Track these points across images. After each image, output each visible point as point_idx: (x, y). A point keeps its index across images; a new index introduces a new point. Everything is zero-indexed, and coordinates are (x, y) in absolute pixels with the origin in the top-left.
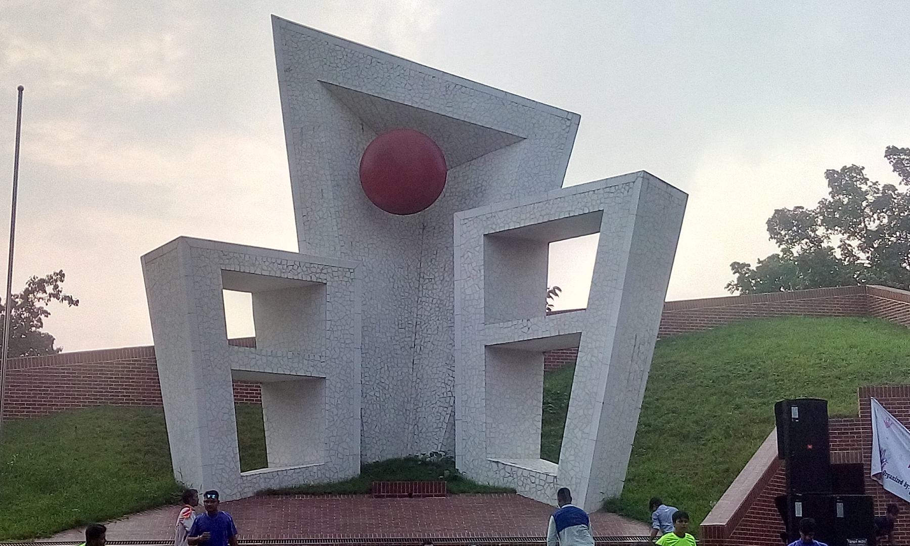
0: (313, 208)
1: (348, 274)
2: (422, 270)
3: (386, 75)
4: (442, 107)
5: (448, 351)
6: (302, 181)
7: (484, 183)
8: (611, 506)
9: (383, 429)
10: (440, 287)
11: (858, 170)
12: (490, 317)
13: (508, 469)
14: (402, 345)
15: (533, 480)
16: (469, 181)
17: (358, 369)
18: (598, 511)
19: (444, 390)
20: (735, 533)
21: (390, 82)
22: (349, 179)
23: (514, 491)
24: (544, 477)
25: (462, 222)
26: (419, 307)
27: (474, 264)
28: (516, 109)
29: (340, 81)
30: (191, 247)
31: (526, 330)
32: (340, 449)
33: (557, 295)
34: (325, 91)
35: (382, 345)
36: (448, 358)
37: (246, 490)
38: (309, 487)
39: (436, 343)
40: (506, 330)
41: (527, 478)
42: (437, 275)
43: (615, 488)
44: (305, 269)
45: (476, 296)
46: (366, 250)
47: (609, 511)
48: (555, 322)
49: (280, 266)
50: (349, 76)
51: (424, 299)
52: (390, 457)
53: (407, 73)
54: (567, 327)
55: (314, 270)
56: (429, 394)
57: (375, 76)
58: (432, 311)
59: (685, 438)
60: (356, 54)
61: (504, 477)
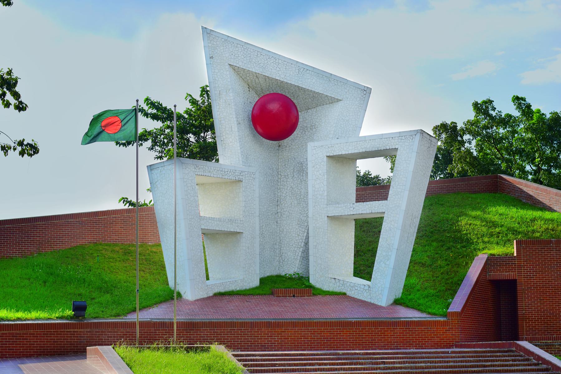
1: (252, 176)
2: (279, 170)
3: (266, 62)
7: (317, 123)
8: (397, 302)
10: (291, 180)
11: (491, 102)
13: (341, 282)
15: (356, 288)
16: (307, 121)
18: (392, 304)
19: (297, 238)
24: (363, 287)
25: (313, 148)
26: (279, 191)
27: (320, 172)
28: (336, 83)
29: (240, 64)
38: (233, 291)
39: (291, 212)
40: (340, 209)
41: (353, 287)
42: (289, 173)
43: (398, 293)
45: (322, 189)
51: (282, 187)
52: (268, 274)
53: (277, 61)
55: (237, 174)
56: (288, 240)
57: (260, 62)
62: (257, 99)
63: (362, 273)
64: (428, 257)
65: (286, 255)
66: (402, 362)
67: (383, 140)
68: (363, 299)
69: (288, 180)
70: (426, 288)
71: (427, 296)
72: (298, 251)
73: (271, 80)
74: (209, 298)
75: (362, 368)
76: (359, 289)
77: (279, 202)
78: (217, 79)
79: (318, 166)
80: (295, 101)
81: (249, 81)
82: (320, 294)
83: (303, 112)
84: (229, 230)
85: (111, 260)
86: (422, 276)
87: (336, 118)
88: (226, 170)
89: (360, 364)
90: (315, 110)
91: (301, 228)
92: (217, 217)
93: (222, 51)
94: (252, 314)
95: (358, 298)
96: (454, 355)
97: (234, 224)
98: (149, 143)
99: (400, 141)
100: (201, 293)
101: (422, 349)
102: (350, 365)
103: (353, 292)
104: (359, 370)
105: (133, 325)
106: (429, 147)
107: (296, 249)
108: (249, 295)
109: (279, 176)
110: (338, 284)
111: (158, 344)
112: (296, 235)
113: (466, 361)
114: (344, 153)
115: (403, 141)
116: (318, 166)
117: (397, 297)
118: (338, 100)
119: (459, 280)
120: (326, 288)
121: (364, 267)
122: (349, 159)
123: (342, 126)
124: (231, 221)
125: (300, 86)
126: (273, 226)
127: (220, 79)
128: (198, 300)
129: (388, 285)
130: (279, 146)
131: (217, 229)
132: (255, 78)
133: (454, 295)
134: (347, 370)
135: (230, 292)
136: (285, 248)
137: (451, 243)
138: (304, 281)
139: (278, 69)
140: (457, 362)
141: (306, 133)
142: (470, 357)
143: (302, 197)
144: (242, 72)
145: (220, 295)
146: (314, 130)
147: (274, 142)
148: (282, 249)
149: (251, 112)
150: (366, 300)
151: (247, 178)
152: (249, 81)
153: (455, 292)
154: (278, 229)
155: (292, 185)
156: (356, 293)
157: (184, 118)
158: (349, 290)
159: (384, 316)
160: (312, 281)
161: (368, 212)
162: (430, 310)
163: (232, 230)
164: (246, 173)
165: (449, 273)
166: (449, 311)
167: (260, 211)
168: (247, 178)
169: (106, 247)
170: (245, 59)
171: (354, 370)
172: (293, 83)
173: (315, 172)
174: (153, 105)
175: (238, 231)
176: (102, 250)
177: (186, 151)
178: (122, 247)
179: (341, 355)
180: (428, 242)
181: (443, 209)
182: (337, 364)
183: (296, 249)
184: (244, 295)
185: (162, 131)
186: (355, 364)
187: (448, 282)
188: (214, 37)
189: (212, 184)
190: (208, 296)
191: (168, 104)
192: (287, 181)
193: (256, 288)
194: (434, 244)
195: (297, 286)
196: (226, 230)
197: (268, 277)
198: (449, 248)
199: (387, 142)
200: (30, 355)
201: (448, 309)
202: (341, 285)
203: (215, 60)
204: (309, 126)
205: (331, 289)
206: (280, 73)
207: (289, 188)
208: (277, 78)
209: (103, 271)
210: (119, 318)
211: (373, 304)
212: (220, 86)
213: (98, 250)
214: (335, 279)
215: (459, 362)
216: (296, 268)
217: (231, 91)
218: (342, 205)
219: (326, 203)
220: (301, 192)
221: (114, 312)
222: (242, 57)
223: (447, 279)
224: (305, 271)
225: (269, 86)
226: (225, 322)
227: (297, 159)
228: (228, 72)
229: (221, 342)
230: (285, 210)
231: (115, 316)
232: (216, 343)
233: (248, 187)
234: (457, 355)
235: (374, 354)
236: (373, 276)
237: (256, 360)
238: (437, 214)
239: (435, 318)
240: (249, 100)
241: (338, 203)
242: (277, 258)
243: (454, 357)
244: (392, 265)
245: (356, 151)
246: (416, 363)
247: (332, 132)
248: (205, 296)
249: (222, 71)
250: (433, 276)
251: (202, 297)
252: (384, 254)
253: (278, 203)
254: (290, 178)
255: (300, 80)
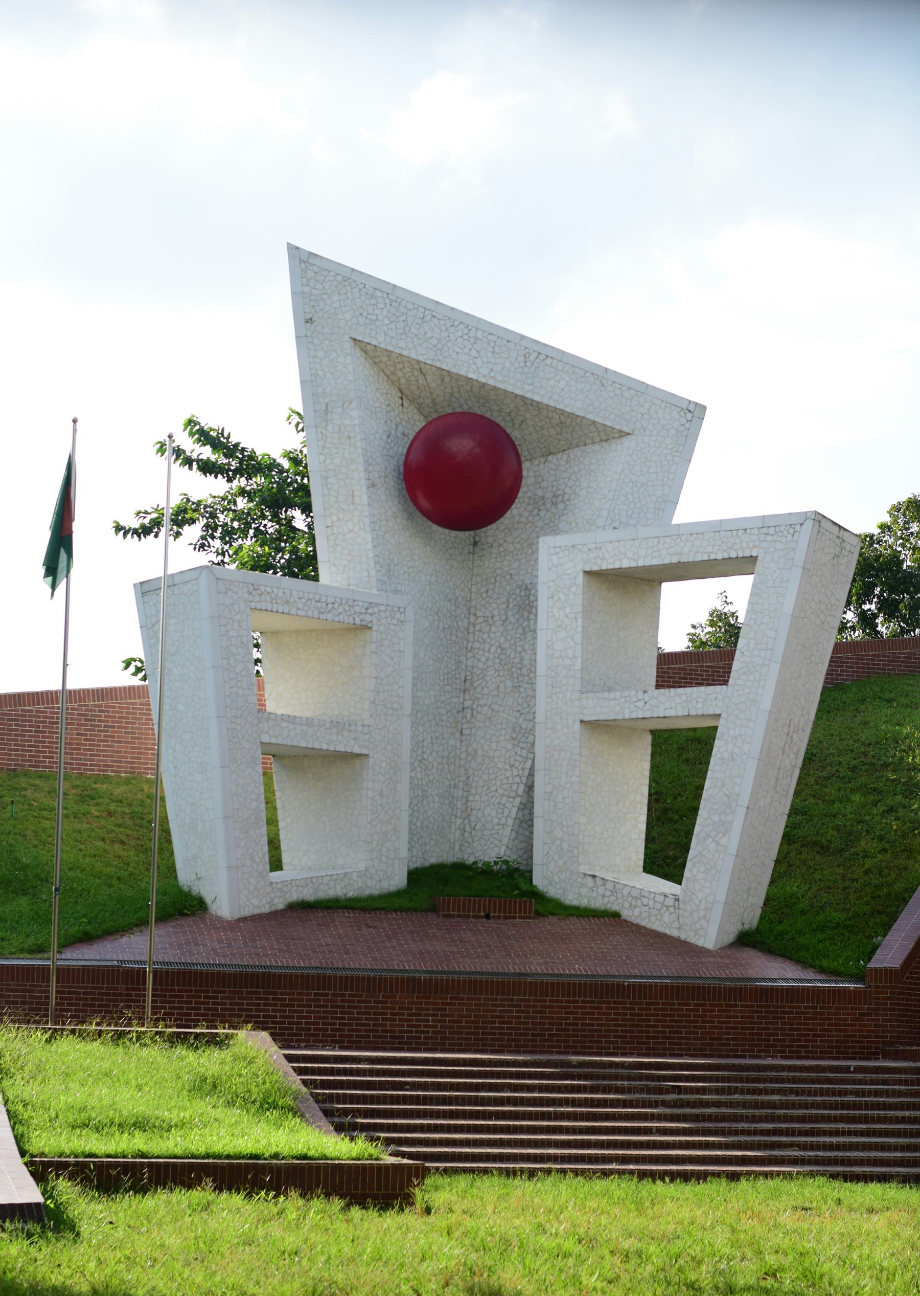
0: (341, 515)
1: (398, 615)
3: (444, 334)
4: (519, 384)
5: (514, 720)
6: (326, 478)
7: (568, 490)
8: (745, 940)
9: (426, 823)
10: (501, 629)
12: (589, 686)
13: (610, 886)
14: (448, 708)
15: (645, 901)
16: (544, 484)
17: (407, 745)
18: (732, 945)
19: (508, 774)
20: (908, 978)
21: (449, 344)
22: (386, 476)
23: (616, 915)
25: (552, 551)
26: (470, 655)
27: (568, 610)
28: (618, 392)
29: (380, 340)
30: (218, 579)
31: (641, 704)
32: (384, 850)
33: (223, 430)
34: (358, 351)
35: (425, 707)
36: (514, 730)
37: (276, 901)
39: (496, 707)
41: (636, 898)
42: (496, 612)
44: (347, 608)
46: (406, 575)
47: (747, 945)
48: (684, 698)
49: (319, 605)
50: (392, 333)
51: (476, 645)
52: (433, 861)
53: (472, 334)
54: (700, 705)
55: (357, 609)
56: (485, 777)
57: (429, 335)
58: (490, 663)
59: (824, 849)
60: (404, 303)
61: (603, 896)
62: (421, 423)
63: (669, 865)
64: (837, 829)
65: (480, 814)
66: (723, 1088)
67: (723, 534)
68: (661, 929)
69: (493, 629)
70: (822, 908)
71: (823, 928)
72: (509, 805)
73: (457, 380)
74: (274, 915)
75: (618, 1100)
76: (651, 904)
77: (468, 684)
78: (321, 373)
79: (562, 596)
80: (515, 434)
81: (403, 381)
82: (553, 914)
83: (536, 462)
84: (332, 748)
85: (45, 813)
86: (817, 876)
87: (617, 477)
88: (330, 600)
89: (618, 1090)
90: (565, 457)
91: (518, 750)
92: (307, 714)
93: (337, 305)
94: (374, 959)
95: (649, 926)
96: (860, 1076)
97: (346, 733)
98: (193, 532)
99: (762, 537)
100: (255, 902)
101: (798, 1058)
102: (592, 1092)
103: (637, 912)
104: (612, 1106)
105: (45, 970)
106: (836, 556)
107: (504, 799)
108: (375, 910)
109: (472, 619)
110: (601, 890)
111: (98, 1024)
112: (507, 767)
113: (888, 1093)
114: (625, 564)
115: (769, 538)
116: (562, 596)
117: (747, 927)
118: (622, 434)
119: (906, 890)
120: (571, 898)
121: (667, 852)
122: (642, 579)
123: (630, 497)
124: (338, 725)
125: (529, 395)
126: (452, 742)
127: (328, 375)
128: (244, 919)
129: (721, 897)
130: (475, 544)
131: (303, 744)
132: (416, 373)
133: (890, 927)
134: (580, 1106)
135: (329, 901)
136: (477, 798)
137: (899, 797)
138: (521, 880)
139: (474, 353)
140: (863, 1093)
141: (542, 513)
142: (900, 1082)
143: (524, 671)
144: (385, 359)
145: (302, 909)
146: (561, 506)
147: (461, 534)
148: (471, 798)
149: (403, 458)
150: (667, 932)
151: (384, 621)
152: (403, 381)
153: (894, 918)
154: (464, 749)
155: (502, 640)
156: (644, 915)
157: (282, 471)
158: (627, 905)
159: (709, 972)
160: (539, 881)
161: (680, 713)
162: (825, 963)
163: (341, 748)
164: (382, 608)
165: (886, 872)
166: (871, 965)
167: (414, 704)
168: (384, 621)
169: (37, 782)
170: (392, 326)
171: (598, 1106)
172: (510, 389)
173: (555, 611)
174: (204, 436)
175: (357, 750)
176: (26, 789)
177: (282, 550)
178: (78, 783)
179: (575, 1067)
180: (842, 792)
181: (889, 712)
182: (559, 1089)
183: (504, 799)
184: (363, 909)
185: (228, 502)
186: (604, 1091)
187: (880, 893)
188: (316, 269)
189: (297, 632)
190: (273, 908)
191: (241, 436)
192: (490, 632)
193: (399, 894)
194: (857, 798)
195: (495, 891)
196: (325, 747)
197: (433, 867)
198: (891, 810)
199: (732, 540)
200: (868, 1053)
201: (870, 960)
202: (608, 893)
203: (319, 328)
204: (549, 495)
205: (584, 902)
206: (479, 363)
207: (493, 649)
208: (471, 375)
209: (21, 839)
210: (39, 956)
211: (685, 944)
212: (328, 391)
213: (15, 789)
214: (594, 876)
215: (870, 1093)
216: (503, 848)
217: (354, 405)
218: (618, 694)
219: (578, 687)
220: (522, 659)
221: (31, 940)
222: (386, 321)
223: (878, 887)
224: (525, 856)
225: (452, 394)
226: (302, 975)
227: (516, 578)
228: (349, 359)
229: (260, 1026)
230: (482, 702)
231: (31, 952)
232: (250, 1025)
233: (386, 643)
234: (869, 1076)
235: (658, 1066)
236: (687, 873)
237: (359, 1072)
238: (872, 724)
239: (836, 982)
240: (400, 429)
241: (610, 690)
242: (459, 821)
243: (860, 1082)
244: (733, 848)
245: (655, 562)
246: (760, 1092)
247: (605, 513)
248: (266, 909)
249: (334, 355)
250: (844, 878)
251: (257, 911)
252: (716, 818)
253: (466, 686)
254: (498, 624)
255: (529, 381)
